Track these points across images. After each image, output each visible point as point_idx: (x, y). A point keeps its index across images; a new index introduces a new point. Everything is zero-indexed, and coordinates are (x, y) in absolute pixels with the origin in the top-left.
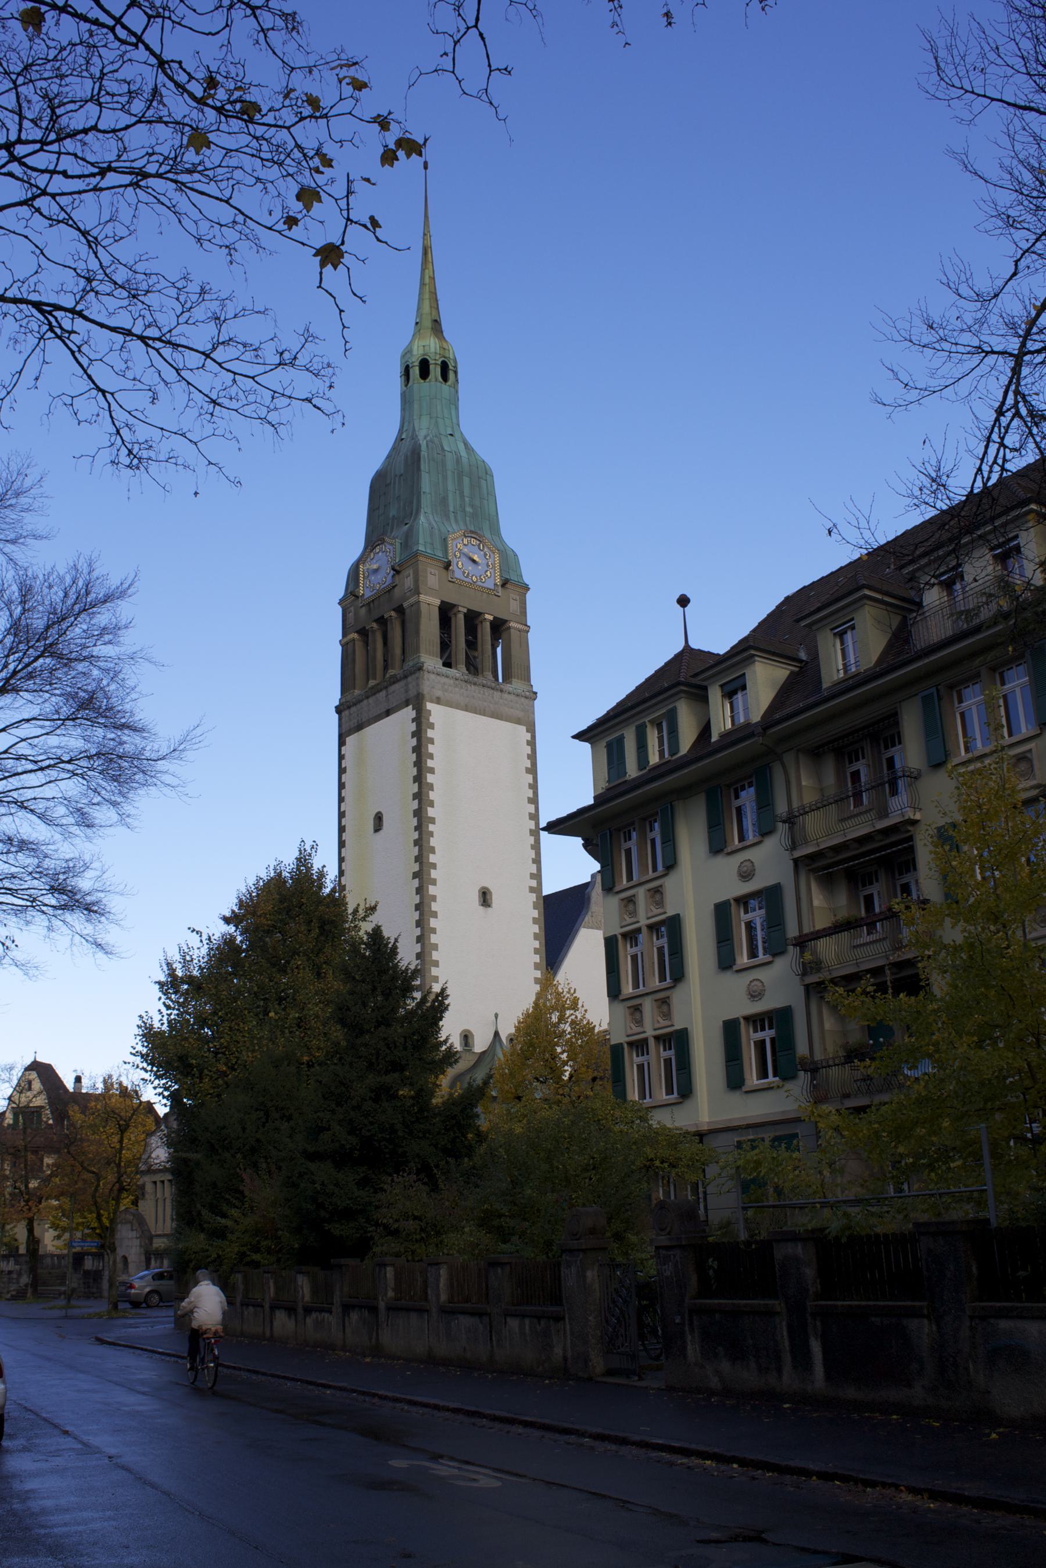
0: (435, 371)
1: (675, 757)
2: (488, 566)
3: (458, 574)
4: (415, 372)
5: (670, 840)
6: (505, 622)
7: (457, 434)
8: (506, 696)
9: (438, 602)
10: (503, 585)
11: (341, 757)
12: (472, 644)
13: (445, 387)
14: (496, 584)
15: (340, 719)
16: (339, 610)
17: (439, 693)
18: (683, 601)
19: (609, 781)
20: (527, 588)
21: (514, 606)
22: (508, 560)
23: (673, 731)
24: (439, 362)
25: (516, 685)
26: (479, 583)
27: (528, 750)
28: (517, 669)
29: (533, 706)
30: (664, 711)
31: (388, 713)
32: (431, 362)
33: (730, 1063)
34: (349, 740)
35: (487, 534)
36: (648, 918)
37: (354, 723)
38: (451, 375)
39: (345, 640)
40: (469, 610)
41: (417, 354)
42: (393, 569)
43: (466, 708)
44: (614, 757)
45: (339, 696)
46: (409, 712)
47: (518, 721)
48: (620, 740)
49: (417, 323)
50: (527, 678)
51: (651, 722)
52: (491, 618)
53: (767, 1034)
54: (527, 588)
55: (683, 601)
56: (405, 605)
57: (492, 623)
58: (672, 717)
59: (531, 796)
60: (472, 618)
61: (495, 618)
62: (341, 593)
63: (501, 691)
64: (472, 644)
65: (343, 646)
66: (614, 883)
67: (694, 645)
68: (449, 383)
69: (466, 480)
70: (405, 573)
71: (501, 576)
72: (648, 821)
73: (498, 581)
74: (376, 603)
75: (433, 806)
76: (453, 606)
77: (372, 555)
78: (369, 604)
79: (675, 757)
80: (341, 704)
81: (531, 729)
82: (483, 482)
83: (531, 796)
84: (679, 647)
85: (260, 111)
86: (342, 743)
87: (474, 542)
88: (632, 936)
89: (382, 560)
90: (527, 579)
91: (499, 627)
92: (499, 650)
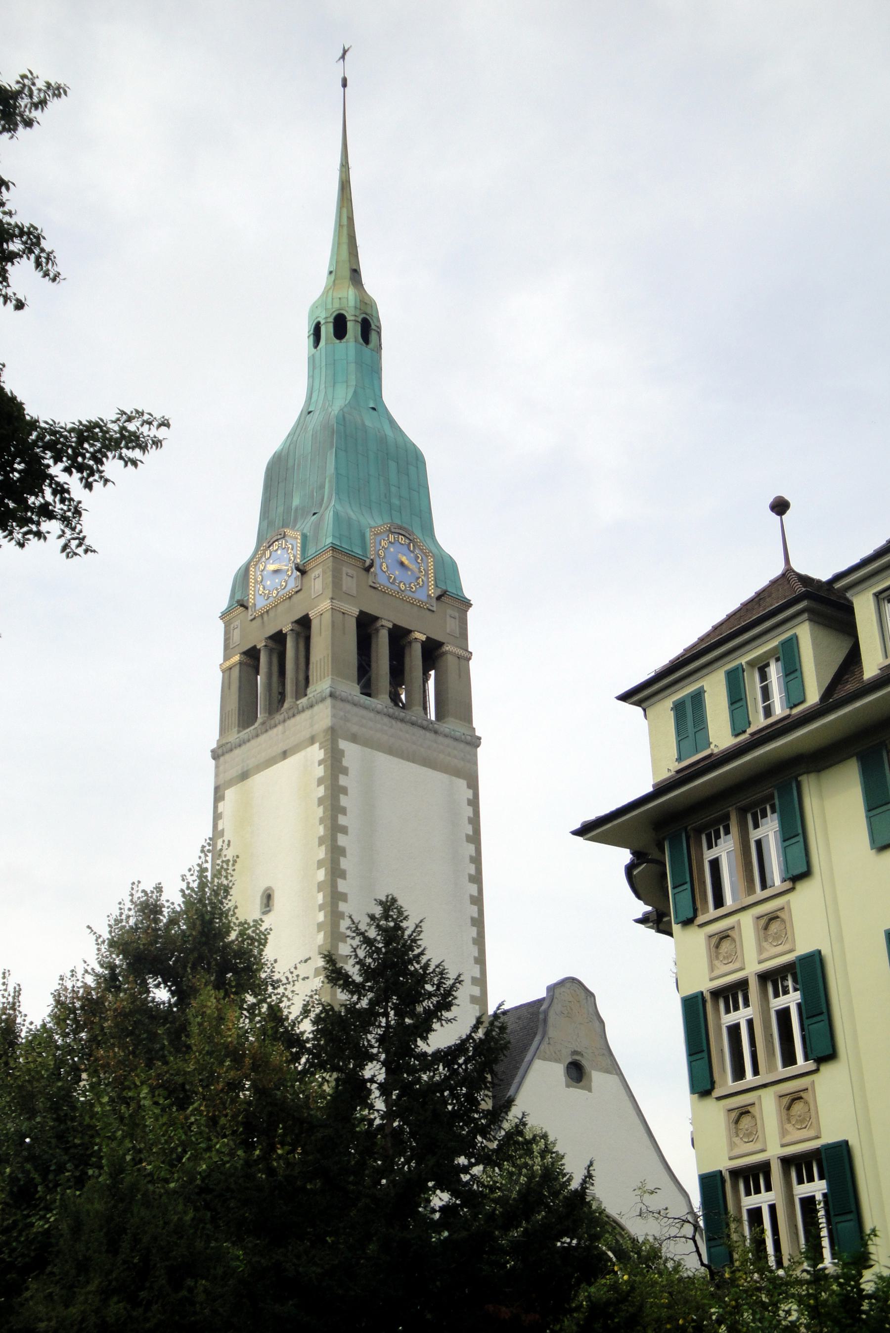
0: (353, 329)
1: (795, 711)
3: (382, 580)
4: (327, 331)
5: (795, 832)
6: (440, 644)
7: (379, 408)
8: (441, 739)
9: (355, 612)
11: (217, 816)
12: (398, 675)
13: (366, 350)
14: (429, 596)
15: (217, 767)
16: (221, 625)
17: (355, 729)
18: (780, 507)
19: (679, 759)
20: (468, 604)
21: (452, 625)
22: (446, 569)
23: (792, 670)
24: (360, 320)
25: (451, 725)
26: (409, 593)
27: (469, 811)
28: (456, 704)
29: (476, 755)
30: (774, 643)
31: (285, 755)
32: (349, 318)
33: (713, 1243)
34: (230, 794)
35: (418, 533)
36: (760, 962)
37: (234, 772)
38: (373, 336)
39: (228, 664)
40: (394, 625)
41: (334, 308)
42: (298, 569)
43: (390, 751)
44: (690, 718)
45: (217, 737)
47: (457, 773)
48: (698, 698)
49: (331, 272)
50: (466, 716)
51: (751, 664)
52: (423, 638)
53: (817, 1188)
54: (468, 604)
55: (780, 507)
56: (312, 615)
57: (424, 644)
58: (789, 655)
60: (399, 637)
61: (428, 638)
62: (223, 603)
63: (436, 732)
64: (398, 675)
65: (223, 672)
66: (695, 911)
67: (800, 568)
68: (371, 345)
69: (393, 465)
70: (312, 574)
71: (436, 586)
72: (754, 812)
74: (272, 614)
75: (344, 878)
76: (376, 619)
77: (268, 554)
78: (262, 615)
79: (795, 711)
80: (220, 746)
81: (473, 783)
82: (412, 470)
83: (473, 872)
84: (778, 570)
85: (51, 504)
86: (218, 796)
87: (402, 540)
88: (731, 994)
89: (283, 558)
90: (468, 593)
91: (432, 653)
92: (431, 684)
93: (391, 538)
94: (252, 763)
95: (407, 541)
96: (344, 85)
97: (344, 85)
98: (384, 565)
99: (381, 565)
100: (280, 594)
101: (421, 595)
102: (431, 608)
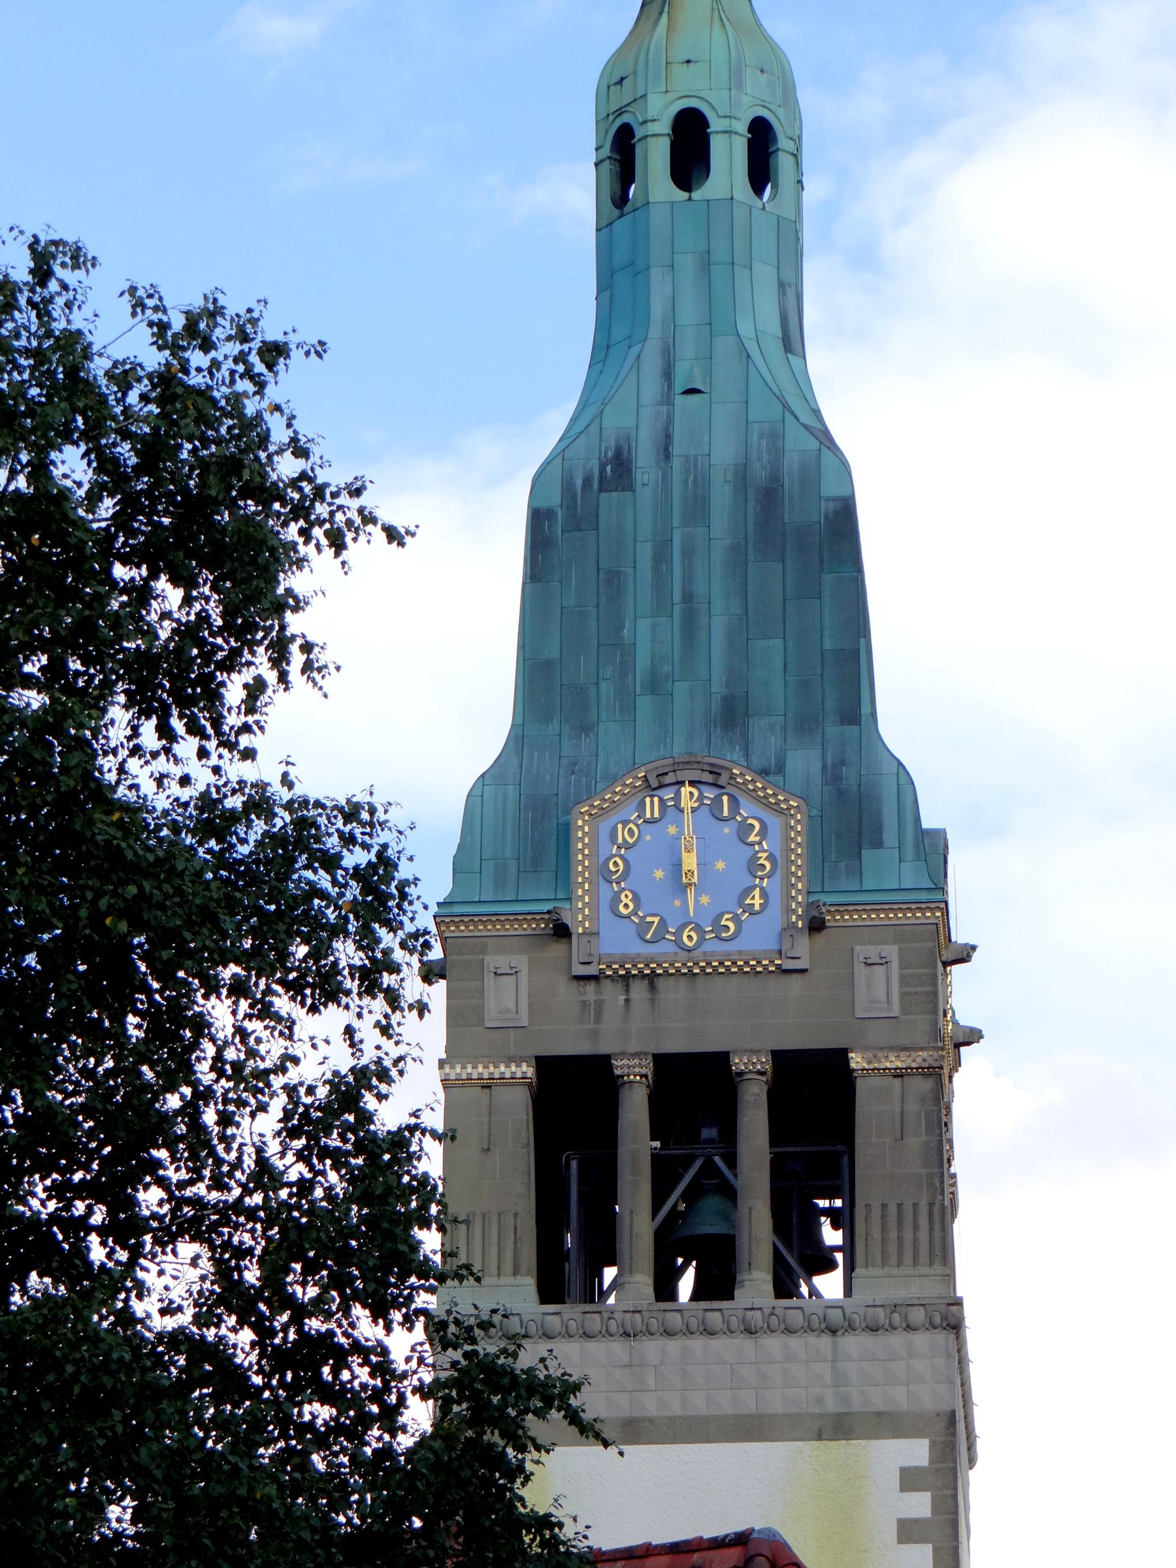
2: (753, 866)
21: (878, 990)
46: (916, 1452)
60: (694, 1088)
93: (652, 807)
95: (710, 793)
98: (626, 898)
99: (616, 899)
100: (707, 947)
101: (759, 937)
102: (789, 965)
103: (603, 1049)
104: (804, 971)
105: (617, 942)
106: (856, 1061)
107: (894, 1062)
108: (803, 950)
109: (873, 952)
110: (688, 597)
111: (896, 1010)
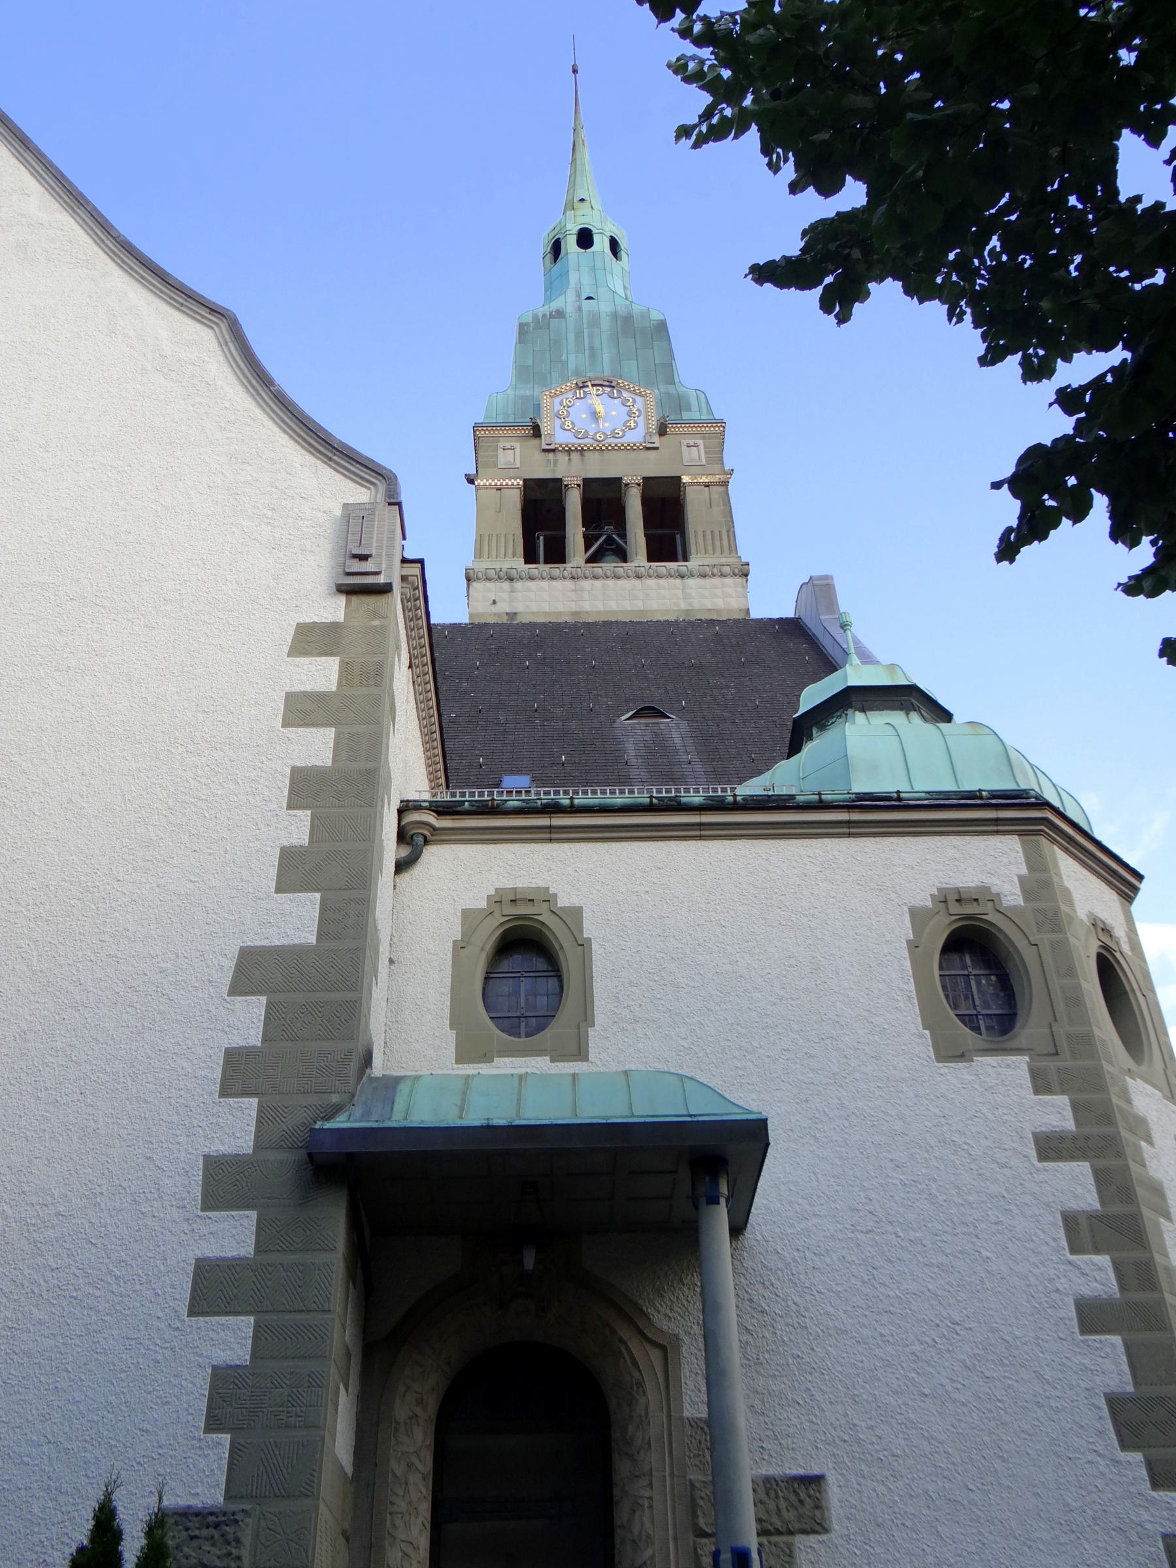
0: (570, 245)
10: (662, 431)
14: (651, 434)
21: (695, 454)
59: (1087, 1198)
73: (654, 424)
83: (1087, 1198)
94: (490, 918)
95: (609, 389)
96: (575, 71)
97: (575, 71)
101: (635, 437)
103: (558, 476)
104: (657, 448)
105: (562, 438)
106: (685, 479)
107: (704, 479)
108: (657, 441)
109: (508, 445)
110: (592, 348)
111: (704, 462)
